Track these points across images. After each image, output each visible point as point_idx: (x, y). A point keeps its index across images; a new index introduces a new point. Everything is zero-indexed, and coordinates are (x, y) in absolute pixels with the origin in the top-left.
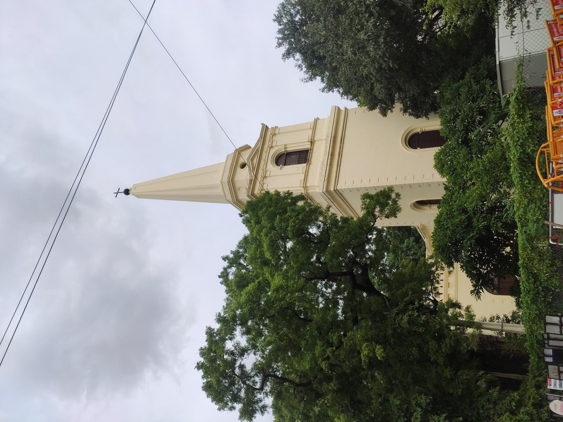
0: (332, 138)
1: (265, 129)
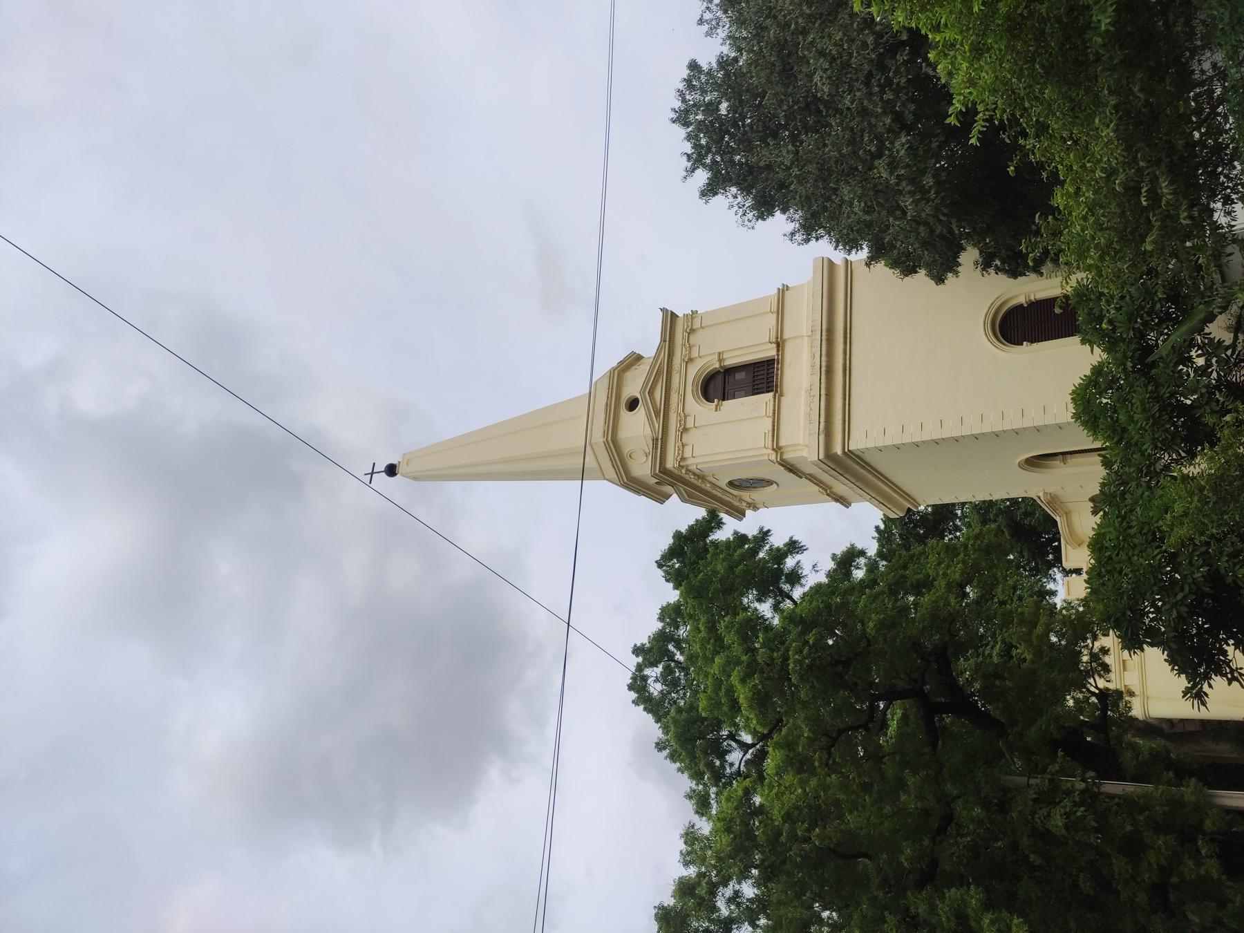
0: (824, 333)
1: (670, 319)
